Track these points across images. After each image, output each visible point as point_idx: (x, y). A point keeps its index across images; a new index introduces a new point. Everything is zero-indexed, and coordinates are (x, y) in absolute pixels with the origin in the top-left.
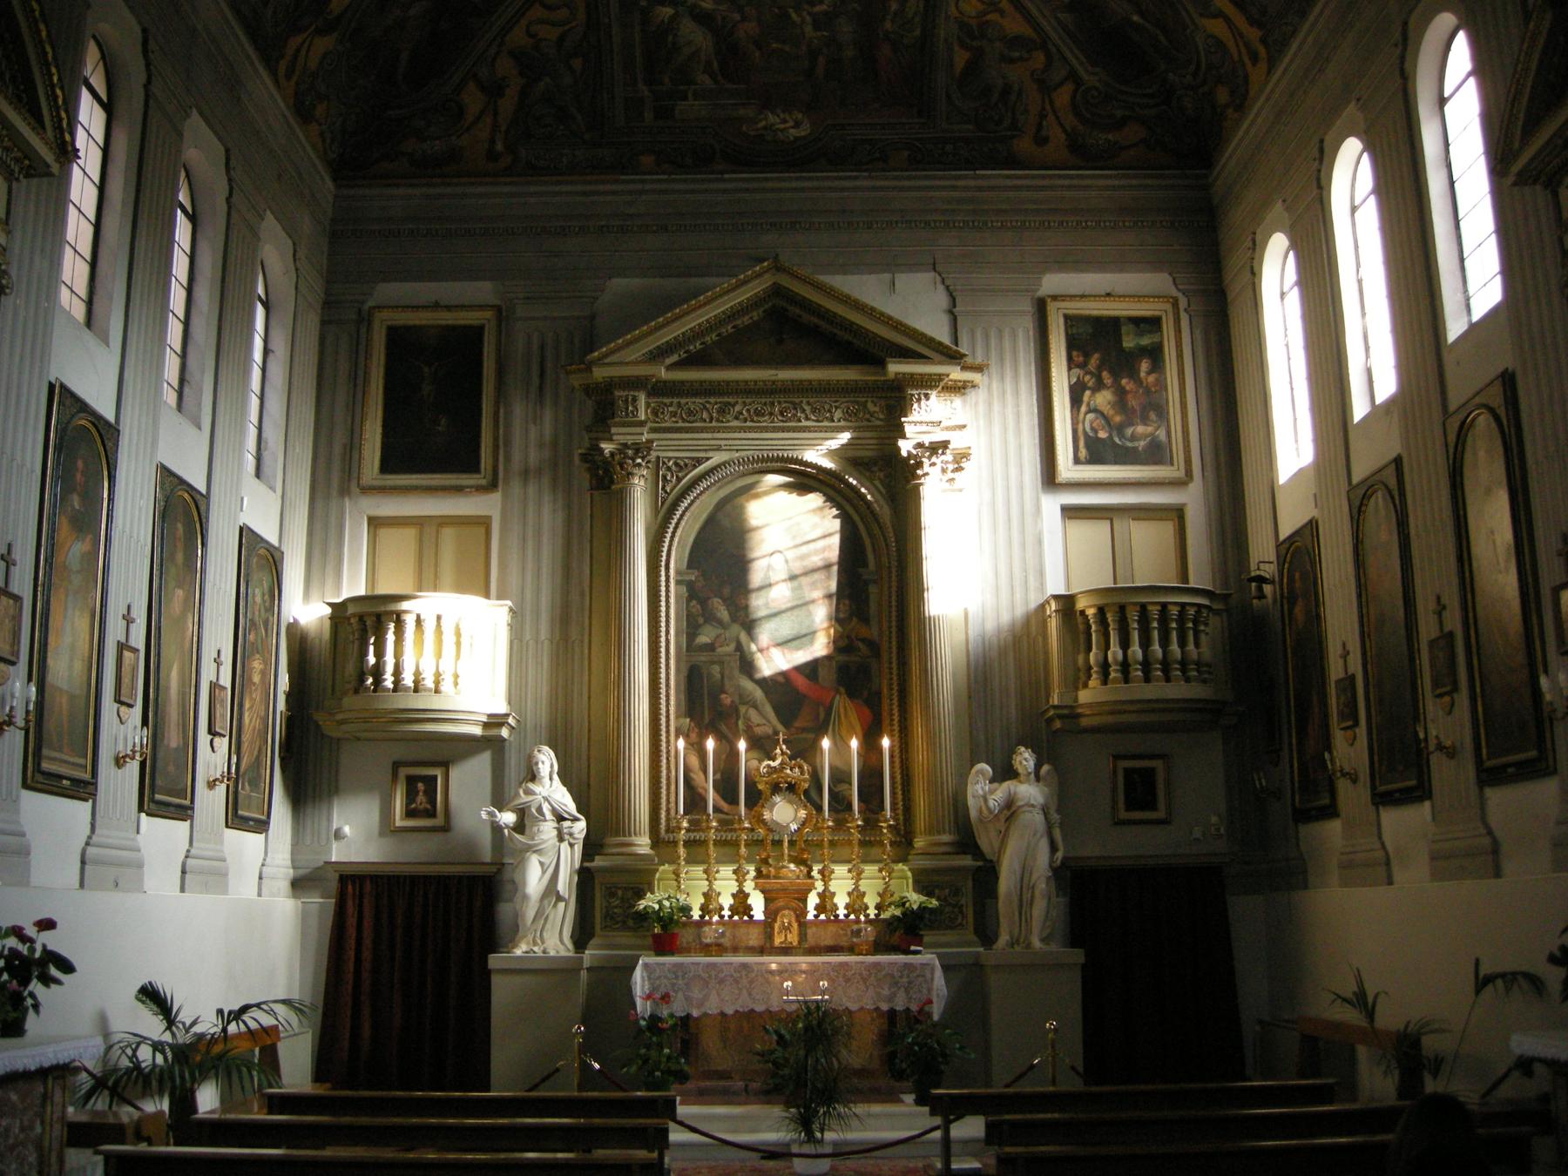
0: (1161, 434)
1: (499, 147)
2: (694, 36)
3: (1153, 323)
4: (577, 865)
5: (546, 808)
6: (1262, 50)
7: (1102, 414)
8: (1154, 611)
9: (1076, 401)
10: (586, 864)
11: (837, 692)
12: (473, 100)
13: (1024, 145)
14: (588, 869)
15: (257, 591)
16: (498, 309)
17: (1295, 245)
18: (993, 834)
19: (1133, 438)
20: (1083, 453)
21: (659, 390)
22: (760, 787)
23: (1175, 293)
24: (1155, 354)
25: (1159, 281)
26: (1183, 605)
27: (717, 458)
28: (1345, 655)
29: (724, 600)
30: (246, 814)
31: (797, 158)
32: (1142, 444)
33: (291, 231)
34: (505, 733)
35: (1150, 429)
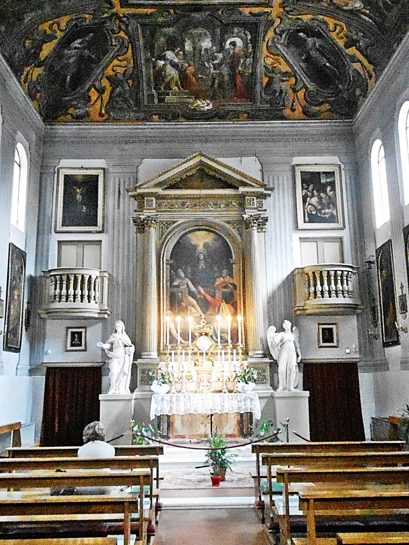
0: (334, 212)
1: (103, 112)
2: (171, 72)
3: (332, 174)
4: (131, 363)
5: (120, 342)
6: (374, 74)
7: (314, 206)
8: (332, 273)
9: (304, 201)
10: (134, 362)
11: (222, 301)
12: (94, 94)
13: (287, 112)
14: (135, 364)
15: (16, 267)
16: (104, 169)
17: (384, 144)
18: (276, 350)
19: (325, 214)
20: (307, 219)
21: (158, 197)
22: (196, 334)
23: (340, 163)
24: (332, 184)
25: (335, 159)
26: (342, 271)
27: (181, 221)
28: (402, 287)
29: (183, 271)
30: (11, 346)
31: (207, 117)
32: (327, 216)
33: (26, 137)
34: (106, 316)
35: (330, 211)
